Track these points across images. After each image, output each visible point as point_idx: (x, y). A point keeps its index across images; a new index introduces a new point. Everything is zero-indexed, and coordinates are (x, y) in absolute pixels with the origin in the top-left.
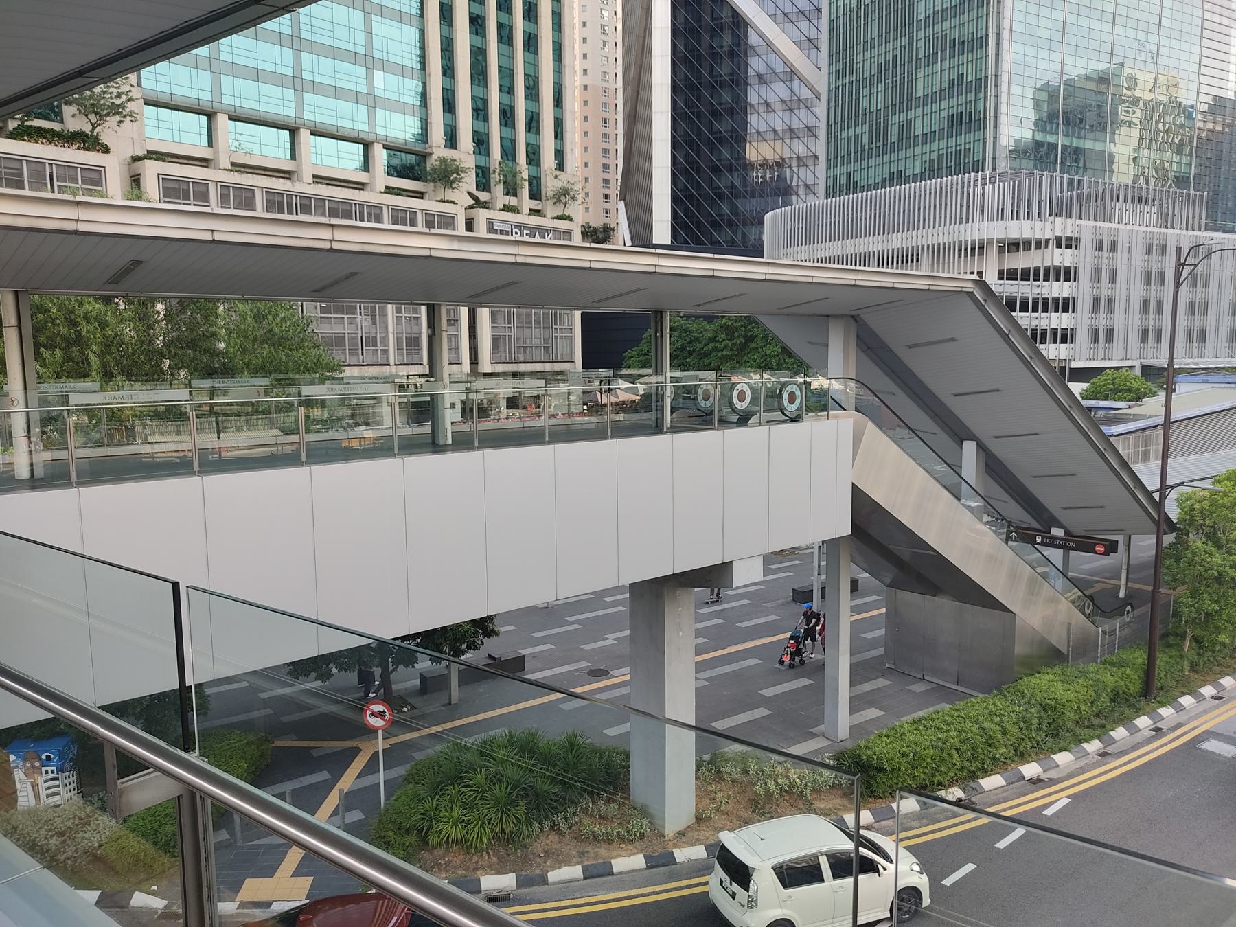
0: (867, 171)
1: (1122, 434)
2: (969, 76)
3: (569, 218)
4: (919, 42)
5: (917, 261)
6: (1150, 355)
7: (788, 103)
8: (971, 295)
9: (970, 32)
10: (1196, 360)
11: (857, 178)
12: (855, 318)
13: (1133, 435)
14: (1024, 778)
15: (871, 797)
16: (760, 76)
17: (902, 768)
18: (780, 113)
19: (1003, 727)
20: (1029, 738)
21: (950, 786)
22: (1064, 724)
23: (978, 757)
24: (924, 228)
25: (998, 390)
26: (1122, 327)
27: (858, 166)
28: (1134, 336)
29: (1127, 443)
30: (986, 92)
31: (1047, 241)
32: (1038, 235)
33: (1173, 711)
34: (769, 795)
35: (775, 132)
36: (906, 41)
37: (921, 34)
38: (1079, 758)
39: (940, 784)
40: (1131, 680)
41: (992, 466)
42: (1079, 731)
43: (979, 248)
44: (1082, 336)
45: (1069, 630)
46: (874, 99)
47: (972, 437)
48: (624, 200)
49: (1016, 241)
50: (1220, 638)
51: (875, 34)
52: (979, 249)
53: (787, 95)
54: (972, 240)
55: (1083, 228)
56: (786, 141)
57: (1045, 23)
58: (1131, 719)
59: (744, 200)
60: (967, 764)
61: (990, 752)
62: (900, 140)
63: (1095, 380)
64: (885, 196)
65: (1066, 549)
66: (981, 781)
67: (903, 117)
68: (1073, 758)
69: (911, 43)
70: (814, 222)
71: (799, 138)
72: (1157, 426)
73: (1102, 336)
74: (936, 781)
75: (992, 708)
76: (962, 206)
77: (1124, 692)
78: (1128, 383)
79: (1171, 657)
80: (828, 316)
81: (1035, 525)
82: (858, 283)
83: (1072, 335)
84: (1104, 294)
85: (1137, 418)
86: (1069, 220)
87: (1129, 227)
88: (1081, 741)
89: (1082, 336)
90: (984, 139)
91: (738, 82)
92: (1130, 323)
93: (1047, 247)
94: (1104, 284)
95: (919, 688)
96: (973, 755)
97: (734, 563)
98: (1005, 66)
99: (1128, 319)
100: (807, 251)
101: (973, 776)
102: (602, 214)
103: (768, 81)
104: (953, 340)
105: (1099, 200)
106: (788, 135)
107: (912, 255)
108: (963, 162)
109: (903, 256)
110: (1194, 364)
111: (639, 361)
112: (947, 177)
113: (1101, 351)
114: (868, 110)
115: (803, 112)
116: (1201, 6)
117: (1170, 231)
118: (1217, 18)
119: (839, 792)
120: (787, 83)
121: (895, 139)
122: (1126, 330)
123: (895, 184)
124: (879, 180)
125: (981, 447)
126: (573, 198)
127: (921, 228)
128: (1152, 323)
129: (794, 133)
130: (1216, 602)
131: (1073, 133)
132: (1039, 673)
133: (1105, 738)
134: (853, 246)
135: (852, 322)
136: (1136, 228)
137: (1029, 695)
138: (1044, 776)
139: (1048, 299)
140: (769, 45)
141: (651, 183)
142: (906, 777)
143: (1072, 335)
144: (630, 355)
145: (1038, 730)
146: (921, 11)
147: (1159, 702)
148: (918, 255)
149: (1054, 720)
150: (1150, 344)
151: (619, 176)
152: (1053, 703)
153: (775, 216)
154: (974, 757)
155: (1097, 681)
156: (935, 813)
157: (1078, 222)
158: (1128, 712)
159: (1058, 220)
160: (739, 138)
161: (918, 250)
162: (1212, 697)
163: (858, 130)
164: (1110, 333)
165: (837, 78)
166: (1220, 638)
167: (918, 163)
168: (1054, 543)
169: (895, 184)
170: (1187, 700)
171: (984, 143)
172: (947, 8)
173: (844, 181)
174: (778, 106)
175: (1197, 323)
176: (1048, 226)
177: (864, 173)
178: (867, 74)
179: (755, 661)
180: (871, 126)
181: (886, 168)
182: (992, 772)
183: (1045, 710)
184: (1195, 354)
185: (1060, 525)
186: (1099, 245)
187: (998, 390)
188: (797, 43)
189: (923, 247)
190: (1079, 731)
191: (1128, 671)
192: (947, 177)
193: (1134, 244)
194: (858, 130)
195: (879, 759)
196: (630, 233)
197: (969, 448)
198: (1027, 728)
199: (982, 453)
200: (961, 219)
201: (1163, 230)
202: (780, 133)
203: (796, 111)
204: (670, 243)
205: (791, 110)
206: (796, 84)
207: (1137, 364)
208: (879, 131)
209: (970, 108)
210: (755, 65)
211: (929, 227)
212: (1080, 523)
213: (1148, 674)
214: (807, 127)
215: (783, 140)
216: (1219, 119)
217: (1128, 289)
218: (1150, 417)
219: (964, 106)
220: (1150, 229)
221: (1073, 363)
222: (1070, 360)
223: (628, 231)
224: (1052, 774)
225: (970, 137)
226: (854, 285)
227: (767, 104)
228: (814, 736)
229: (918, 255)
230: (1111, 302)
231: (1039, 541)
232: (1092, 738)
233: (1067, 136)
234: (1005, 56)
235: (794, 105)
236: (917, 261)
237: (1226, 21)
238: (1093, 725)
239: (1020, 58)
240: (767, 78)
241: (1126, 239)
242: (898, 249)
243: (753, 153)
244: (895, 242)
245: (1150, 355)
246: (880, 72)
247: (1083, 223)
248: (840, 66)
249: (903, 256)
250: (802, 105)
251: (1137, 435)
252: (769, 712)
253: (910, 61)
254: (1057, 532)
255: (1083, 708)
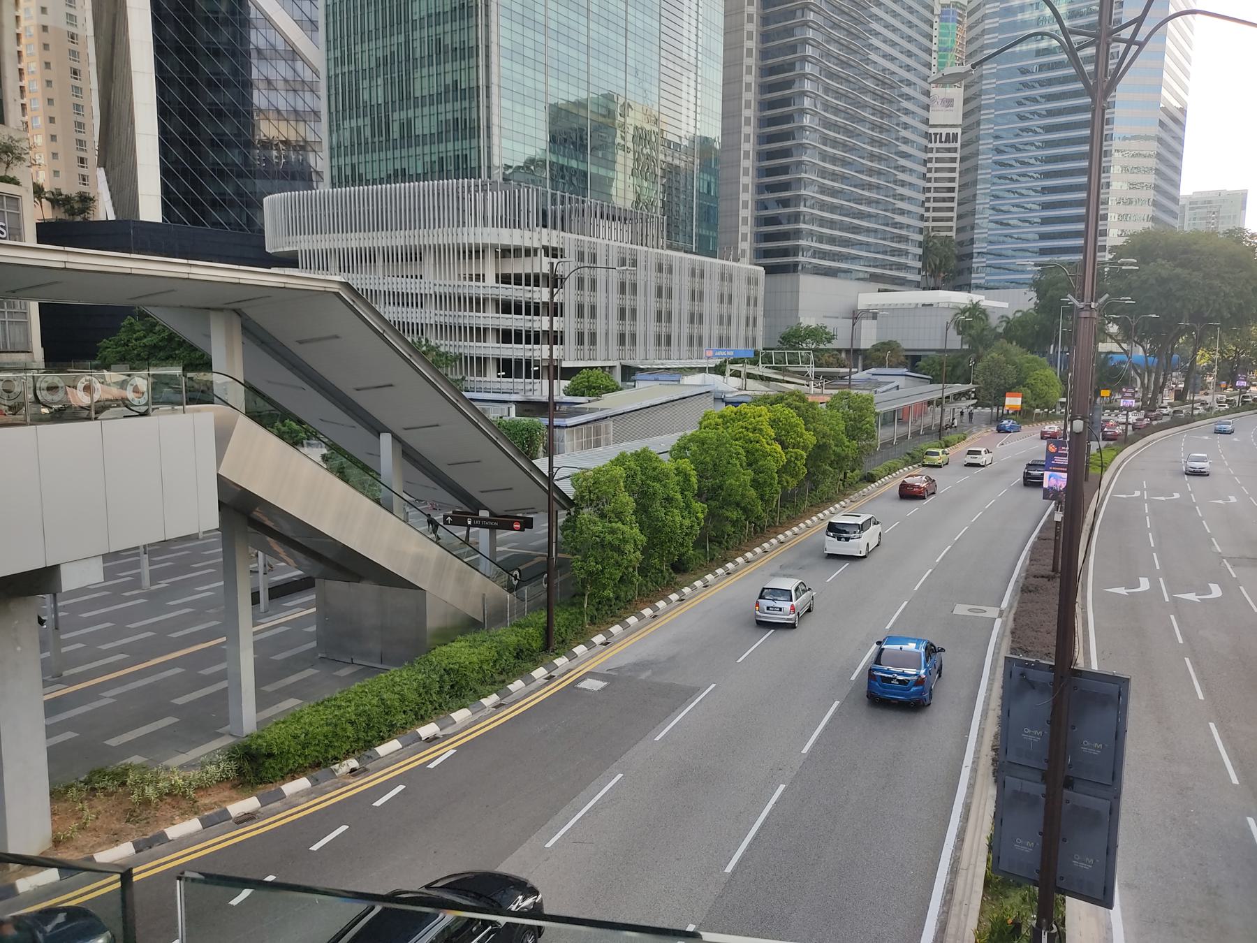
0: (371, 164)
1: (576, 425)
2: (463, 83)
3: (14, 181)
4: (415, 42)
5: (421, 260)
6: (627, 357)
7: (292, 83)
8: (337, 294)
9: (462, 39)
10: (664, 361)
11: (362, 171)
12: (238, 312)
13: (585, 426)
14: (421, 738)
15: (261, 783)
16: (259, 51)
17: (292, 750)
18: (283, 93)
19: (402, 695)
20: (430, 701)
21: (345, 759)
22: (468, 683)
23: (373, 726)
24: (425, 228)
25: (391, 385)
26: (604, 332)
27: (362, 158)
28: (614, 340)
29: (580, 433)
30: (478, 102)
31: (536, 250)
32: (527, 243)
33: (567, 660)
34: (146, 802)
35: (278, 111)
36: (402, 38)
37: (417, 34)
38: (476, 713)
39: (336, 758)
40: (534, 639)
41: (408, 453)
42: (480, 688)
43: (475, 252)
44: (570, 338)
45: (483, 599)
46: (375, 92)
47: (387, 431)
48: (104, 167)
49: (509, 248)
50: (606, 593)
51: (372, 27)
52: (477, 252)
53: (290, 75)
54: (469, 244)
55: (566, 239)
56: (291, 122)
57: (529, 43)
58: (529, 671)
59: (247, 180)
60: (362, 735)
61: (387, 720)
62: (402, 137)
63: (574, 378)
64: (386, 192)
65: (492, 528)
66: (377, 749)
67: (403, 115)
68: (470, 713)
69: (407, 42)
70: (359, 207)
71: (305, 121)
72: (607, 417)
73: (586, 339)
74: (330, 757)
75: (397, 679)
76: (458, 209)
77: (528, 650)
78: (600, 381)
79: (571, 614)
80: (209, 309)
81: (466, 509)
82: (191, 276)
83: (561, 337)
84: (587, 301)
85: (591, 411)
86: (554, 231)
87: (606, 242)
88: (480, 698)
89: (570, 338)
90: (479, 147)
91: (239, 53)
92: (610, 327)
93: (536, 254)
94: (587, 292)
95: (345, 672)
96: (368, 725)
97: (63, 568)
98: (494, 79)
99: (608, 325)
100: (311, 241)
101: (369, 745)
102: (77, 180)
103: (268, 57)
104: (337, 337)
105: (573, 216)
106: (292, 117)
107: (416, 254)
108: (464, 167)
109: (411, 254)
110: (662, 364)
111: (118, 352)
112: (447, 180)
113: (587, 352)
114: (368, 103)
115: (308, 96)
116: (628, 58)
117: (639, 247)
118: (671, 65)
119: (229, 785)
120: (290, 62)
121: (397, 135)
122: (607, 334)
123: (414, 179)
124: (383, 175)
125: (395, 438)
126: (19, 158)
127: (422, 227)
128: (628, 328)
129: (282, 115)
130: (601, 563)
131: (559, 151)
132: (453, 641)
133: (502, 691)
134: (371, 239)
135: (235, 316)
136: (612, 243)
137: (436, 663)
138: (440, 734)
139: (538, 303)
140: (267, 19)
141: (135, 151)
142: (297, 758)
143: (561, 337)
144: (105, 345)
145: (440, 693)
146: (419, 10)
147: (557, 654)
148: (421, 254)
149: (457, 682)
150: (627, 347)
151: (97, 138)
152: (456, 667)
153: (273, 201)
154: (369, 727)
155: (501, 642)
156: (326, 787)
157: (562, 234)
158: (529, 665)
159: (544, 230)
160: (243, 113)
161: (420, 249)
162: (602, 644)
163: (361, 122)
164: (593, 336)
165: (336, 65)
166: (606, 593)
167: (420, 164)
168: (481, 524)
169: (414, 179)
170: (580, 650)
171: (479, 151)
172: (439, 12)
173: (349, 172)
174: (281, 85)
175: (664, 329)
176: (536, 235)
177: (369, 166)
178: (366, 66)
179: (178, 670)
180: (372, 120)
181: (390, 163)
182: (390, 738)
183: (449, 674)
184: (663, 356)
185: (486, 509)
186: (581, 257)
187: (391, 385)
188: (299, 22)
189: (425, 246)
190: (480, 688)
191: (531, 630)
192: (463, 179)
193: (611, 258)
194: (361, 122)
195: (269, 745)
196: (113, 205)
197: (386, 439)
198: (426, 693)
199: (399, 446)
200: (458, 222)
201: (634, 247)
202: (285, 114)
203: (301, 93)
204: (161, 221)
205: (295, 91)
206: (299, 65)
207: (617, 364)
208: (381, 126)
209: (465, 115)
210: (257, 39)
211: (429, 228)
212: (501, 504)
213: (548, 631)
214: (313, 111)
215: (288, 121)
216: (676, 154)
217: (607, 297)
218: (602, 410)
219: (459, 112)
220: (623, 245)
221: (563, 362)
222: (561, 360)
223: (110, 203)
224: (448, 731)
225: (466, 144)
226: (188, 279)
227: (269, 81)
228: (222, 735)
229: (421, 254)
230: (593, 308)
231: (469, 523)
232: (490, 693)
233: (554, 153)
234: (494, 68)
235: (298, 87)
236: (421, 260)
237: (678, 69)
238: (495, 682)
239: (508, 73)
240: (268, 53)
241: (604, 252)
242: (402, 246)
243: (267, 129)
244: (398, 239)
245: (627, 357)
246: (378, 66)
247: (567, 235)
248: (338, 54)
249: (411, 254)
250: (306, 88)
251: (589, 425)
252: (177, 720)
253: (407, 60)
254: (484, 514)
255: (485, 667)
